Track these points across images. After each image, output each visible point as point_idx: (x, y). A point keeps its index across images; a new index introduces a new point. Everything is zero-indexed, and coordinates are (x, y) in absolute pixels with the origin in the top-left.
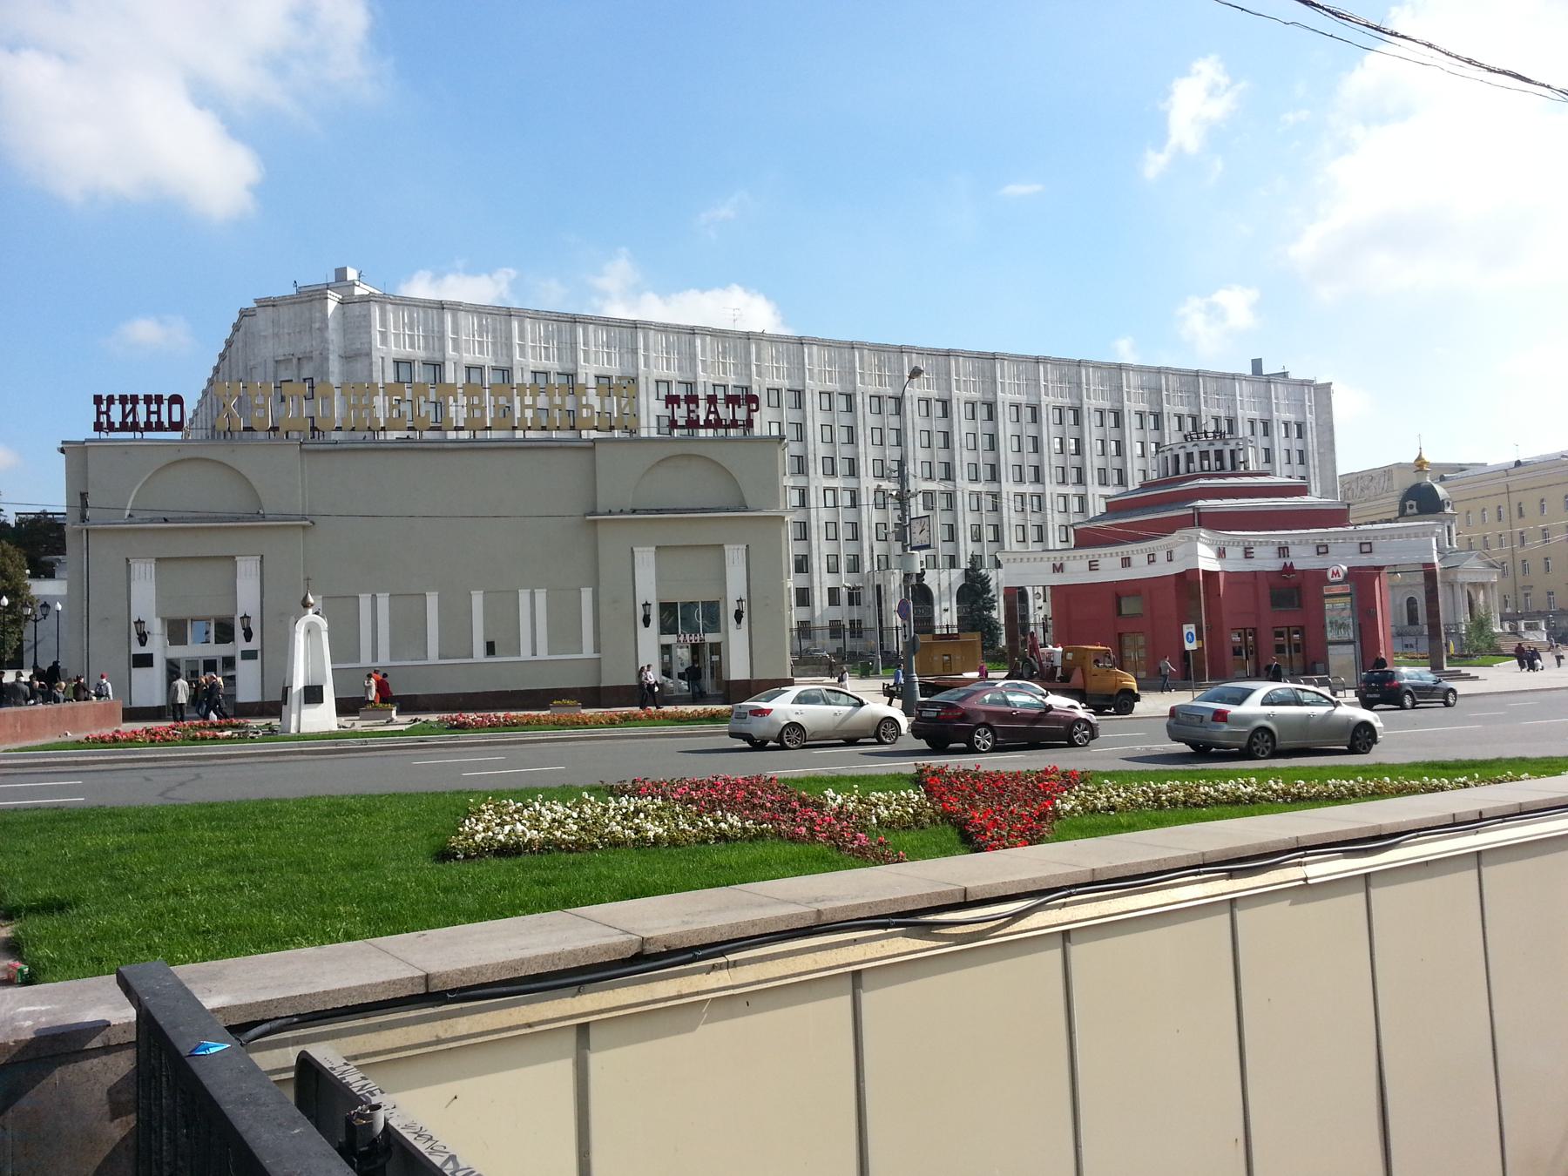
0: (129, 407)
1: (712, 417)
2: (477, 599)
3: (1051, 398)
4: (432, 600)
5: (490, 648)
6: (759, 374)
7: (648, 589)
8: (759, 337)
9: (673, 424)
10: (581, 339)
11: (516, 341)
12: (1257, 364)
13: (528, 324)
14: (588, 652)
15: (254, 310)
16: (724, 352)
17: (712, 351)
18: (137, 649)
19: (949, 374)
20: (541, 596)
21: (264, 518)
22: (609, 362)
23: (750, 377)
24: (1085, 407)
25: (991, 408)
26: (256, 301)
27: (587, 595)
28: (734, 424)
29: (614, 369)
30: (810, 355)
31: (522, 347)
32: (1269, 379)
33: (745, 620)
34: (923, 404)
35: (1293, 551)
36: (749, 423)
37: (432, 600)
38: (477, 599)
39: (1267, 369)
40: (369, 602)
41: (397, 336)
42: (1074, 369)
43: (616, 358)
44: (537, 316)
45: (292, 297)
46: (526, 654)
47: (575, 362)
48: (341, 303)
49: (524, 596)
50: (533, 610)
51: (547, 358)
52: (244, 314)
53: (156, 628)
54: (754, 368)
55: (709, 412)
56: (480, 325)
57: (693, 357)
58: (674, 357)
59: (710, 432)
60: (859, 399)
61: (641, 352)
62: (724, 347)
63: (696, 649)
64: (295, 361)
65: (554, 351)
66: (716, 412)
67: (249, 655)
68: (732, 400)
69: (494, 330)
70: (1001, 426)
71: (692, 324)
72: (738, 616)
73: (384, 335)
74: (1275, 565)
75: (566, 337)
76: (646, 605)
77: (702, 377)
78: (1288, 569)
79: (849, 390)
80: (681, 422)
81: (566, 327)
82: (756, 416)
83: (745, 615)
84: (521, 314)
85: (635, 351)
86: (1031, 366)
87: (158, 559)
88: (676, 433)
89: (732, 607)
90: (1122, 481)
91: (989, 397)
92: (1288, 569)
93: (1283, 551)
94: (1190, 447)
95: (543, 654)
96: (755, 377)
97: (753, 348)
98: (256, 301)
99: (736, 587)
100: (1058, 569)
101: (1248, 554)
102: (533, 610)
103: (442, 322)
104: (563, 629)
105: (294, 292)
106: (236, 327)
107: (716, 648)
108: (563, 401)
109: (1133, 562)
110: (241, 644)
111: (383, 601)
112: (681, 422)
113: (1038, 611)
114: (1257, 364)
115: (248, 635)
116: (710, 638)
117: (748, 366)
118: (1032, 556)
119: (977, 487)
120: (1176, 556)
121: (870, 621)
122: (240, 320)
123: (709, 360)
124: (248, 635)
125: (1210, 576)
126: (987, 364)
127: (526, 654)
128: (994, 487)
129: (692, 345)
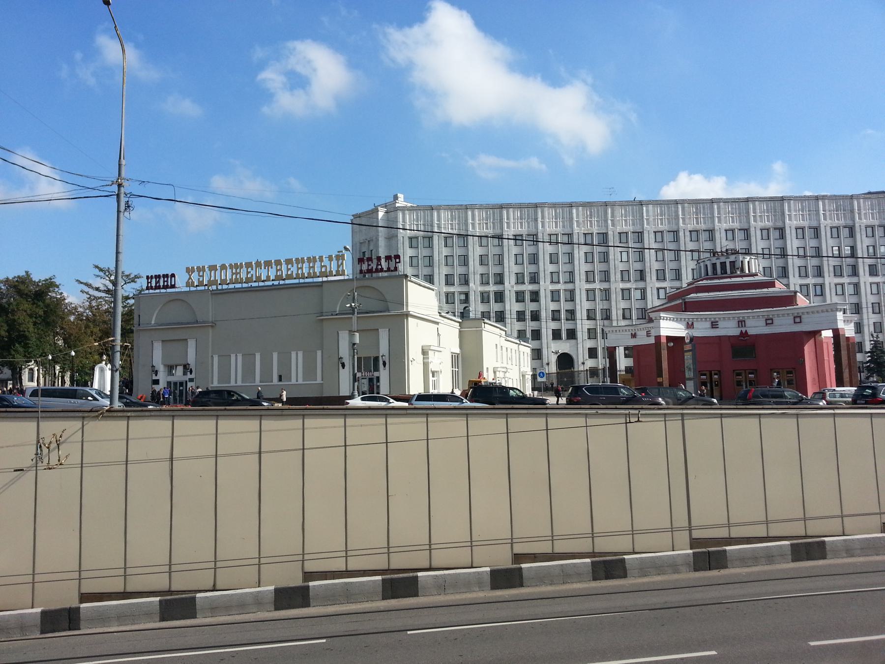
0: (340, 269)
2: (275, 356)
3: (829, 222)
5: (280, 378)
6: (613, 225)
8: (718, 201)
10: (575, 215)
11: (470, 221)
13: (476, 212)
14: (319, 381)
16: (591, 215)
17: (583, 214)
18: (154, 378)
19: (748, 213)
20: (300, 354)
21: (197, 322)
22: (521, 227)
23: (607, 227)
24: (857, 225)
25: (782, 231)
27: (319, 353)
29: (524, 230)
30: (647, 211)
31: (473, 224)
33: (387, 366)
35: (749, 323)
38: (275, 356)
41: (514, 223)
42: (847, 202)
43: (525, 225)
44: (622, 204)
46: (294, 381)
47: (819, 221)
48: (386, 212)
49: (293, 355)
51: (487, 228)
53: (161, 368)
54: (610, 222)
56: (452, 215)
57: (571, 219)
58: (560, 221)
60: (681, 234)
61: (540, 220)
62: (591, 212)
63: (371, 380)
65: (490, 225)
69: (459, 217)
70: (789, 242)
71: (569, 201)
73: (473, 224)
74: (735, 332)
75: (497, 216)
77: (576, 229)
79: (674, 228)
81: (497, 211)
84: (613, 204)
85: (536, 220)
86: (812, 203)
90: (678, 276)
91: (780, 224)
92: (744, 334)
93: (741, 323)
95: (300, 381)
96: (610, 227)
97: (609, 211)
100: (634, 336)
101: (714, 325)
103: (432, 216)
107: (378, 379)
116: (376, 374)
117: (606, 221)
118: (621, 329)
119: (521, 288)
123: (581, 220)
125: (676, 341)
126: (778, 204)
127: (294, 381)
128: (819, 280)
129: (571, 213)
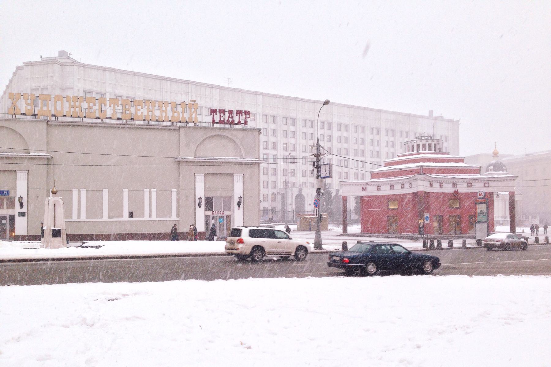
1: (230, 119)
4: (106, 193)
5: (131, 215)
7: (200, 192)
9: (214, 122)
12: (431, 112)
15: (22, 67)
26: (24, 63)
28: (239, 123)
32: (436, 119)
33: (241, 206)
34: (303, 121)
35: (429, 185)
36: (246, 123)
37: (106, 193)
39: (435, 115)
40: (77, 192)
45: (39, 62)
46: (147, 218)
50: (150, 198)
52: (19, 68)
55: (229, 117)
59: (218, 126)
64: (40, 89)
66: (232, 117)
67: (22, 214)
68: (239, 113)
72: (239, 204)
76: (200, 198)
78: (456, 192)
80: (217, 121)
82: (248, 120)
83: (242, 204)
87: (206, 175)
88: (215, 125)
89: (236, 200)
92: (456, 192)
94: (419, 142)
98: (24, 63)
99: (238, 191)
102: (150, 198)
104: (164, 208)
105: (40, 60)
106: (15, 74)
108: (148, 113)
109: (395, 188)
110: (18, 209)
111: (83, 193)
112: (217, 121)
113: (352, 205)
114: (431, 112)
115: (22, 205)
120: (413, 186)
121: (279, 208)
122: (16, 71)
124: (22, 205)
